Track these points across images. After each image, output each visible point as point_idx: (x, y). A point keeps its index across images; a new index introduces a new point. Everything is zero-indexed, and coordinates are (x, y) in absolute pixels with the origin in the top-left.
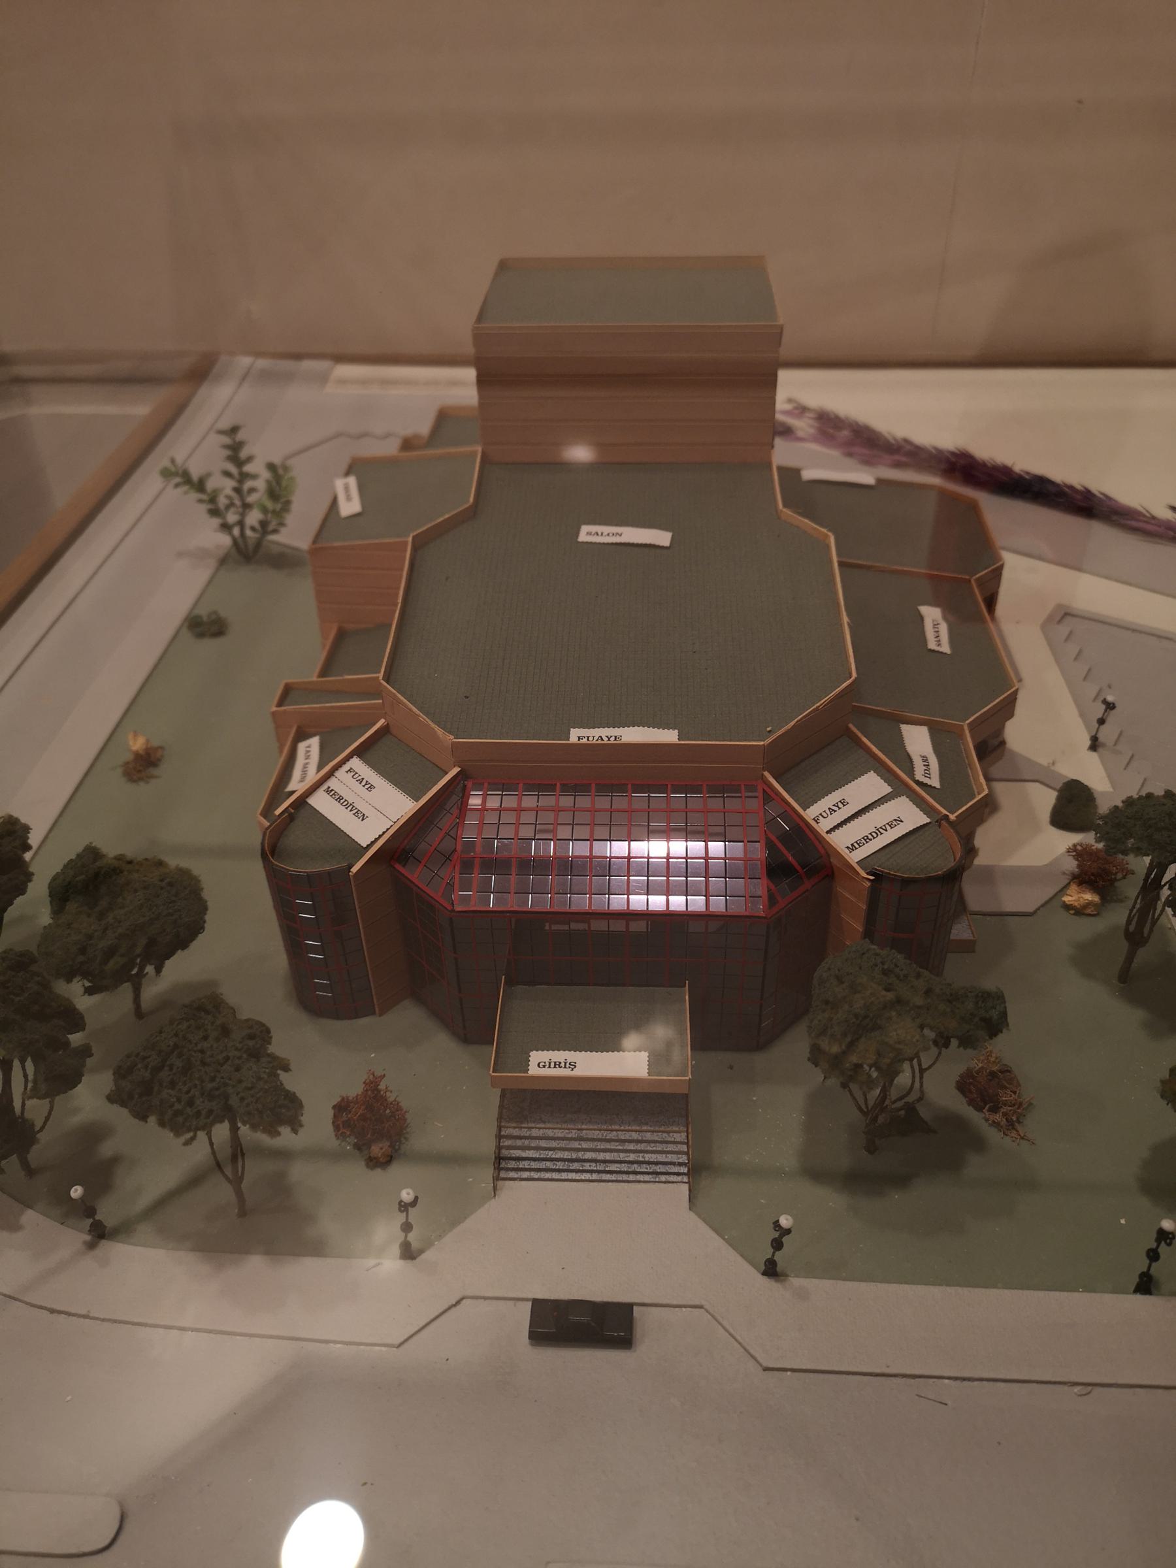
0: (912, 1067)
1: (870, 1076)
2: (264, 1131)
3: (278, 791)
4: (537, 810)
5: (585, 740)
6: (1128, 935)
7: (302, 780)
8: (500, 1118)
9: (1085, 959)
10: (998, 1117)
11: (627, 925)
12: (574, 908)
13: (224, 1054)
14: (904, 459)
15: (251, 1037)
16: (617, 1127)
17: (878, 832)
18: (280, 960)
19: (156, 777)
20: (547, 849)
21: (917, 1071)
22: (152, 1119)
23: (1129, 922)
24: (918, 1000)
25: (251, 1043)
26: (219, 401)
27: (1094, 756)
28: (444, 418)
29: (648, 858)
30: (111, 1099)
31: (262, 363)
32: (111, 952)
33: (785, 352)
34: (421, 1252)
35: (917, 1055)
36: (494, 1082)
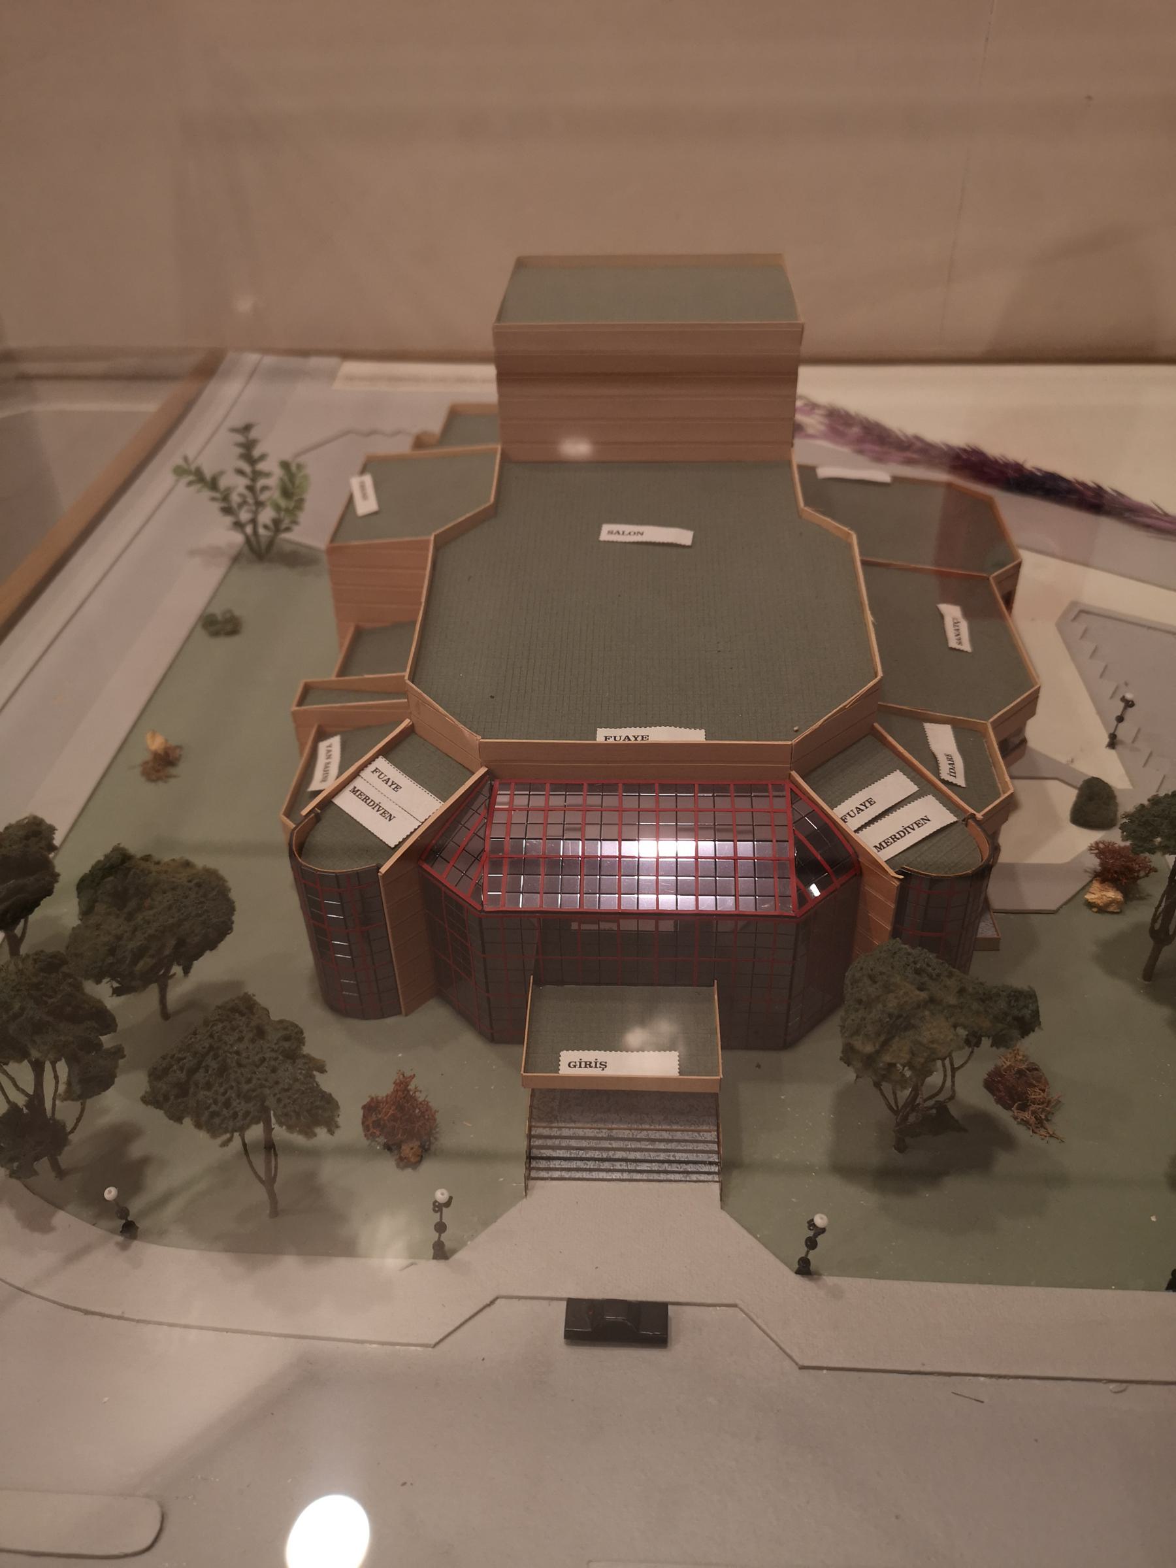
0: (944, 1066)
1: (903, 1075)
2: (300, 1132)
3: (301, 792)
4: (565, 809)
5: (612, 740)
6: (1153, 933)
7: (324, 780)
8: (531, 1119)
9: (1109, 956)
10: (1026, 1115)
11: (657, 926)
12: (604, 907)
13: (260, 1055)
14: (915, 456)
15: (287, 1038)
16: (647, 1127)
17: (906, 831)
18: (305, 959)
19: (175, 776)
20: (575, 849)
21: (949, 1073)
22: (188, 1121)
23: (1154, 920)
24: (952, 1000)
25: (287, 1045)
26: (229, 398)
27: (1113, 753)
28: (456, 415)
29: (677, 857)
30: (145, 1100)
31: (269, 360)
32: (139, 954)
33: (806, 349)
34: (454, 1252)
35: (950, 1055)
36: (525, 1082)
